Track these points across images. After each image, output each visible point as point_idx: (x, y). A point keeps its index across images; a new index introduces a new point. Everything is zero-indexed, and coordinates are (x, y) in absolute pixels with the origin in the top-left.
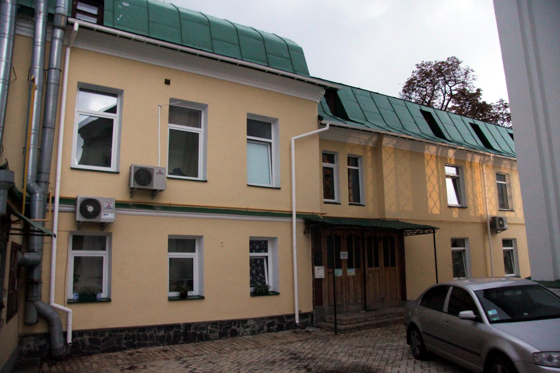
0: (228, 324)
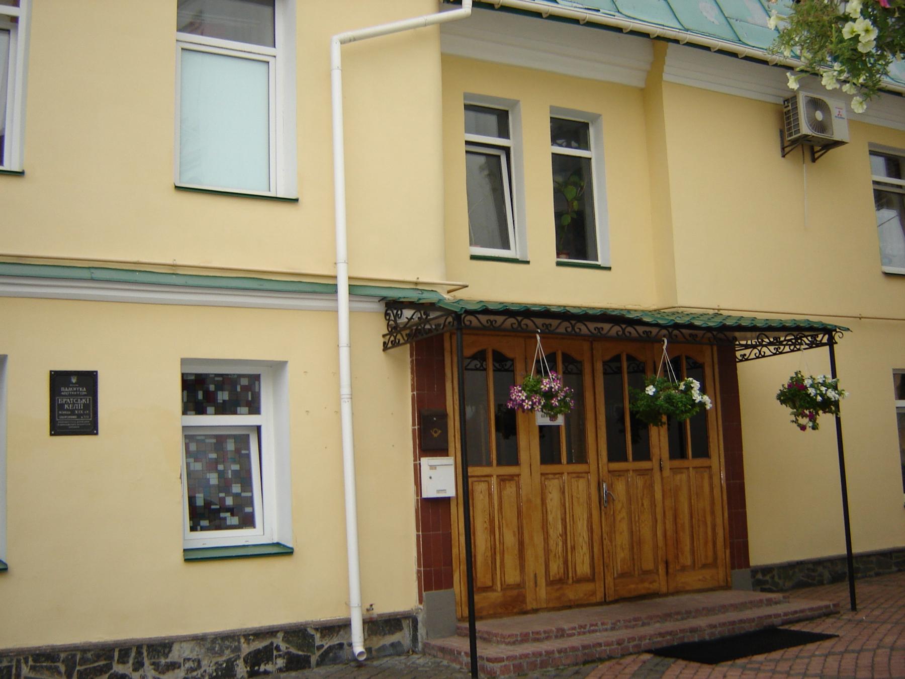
0: (98, 657)
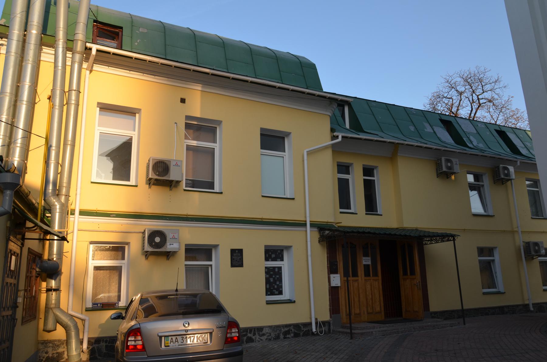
0: (244, 331)
